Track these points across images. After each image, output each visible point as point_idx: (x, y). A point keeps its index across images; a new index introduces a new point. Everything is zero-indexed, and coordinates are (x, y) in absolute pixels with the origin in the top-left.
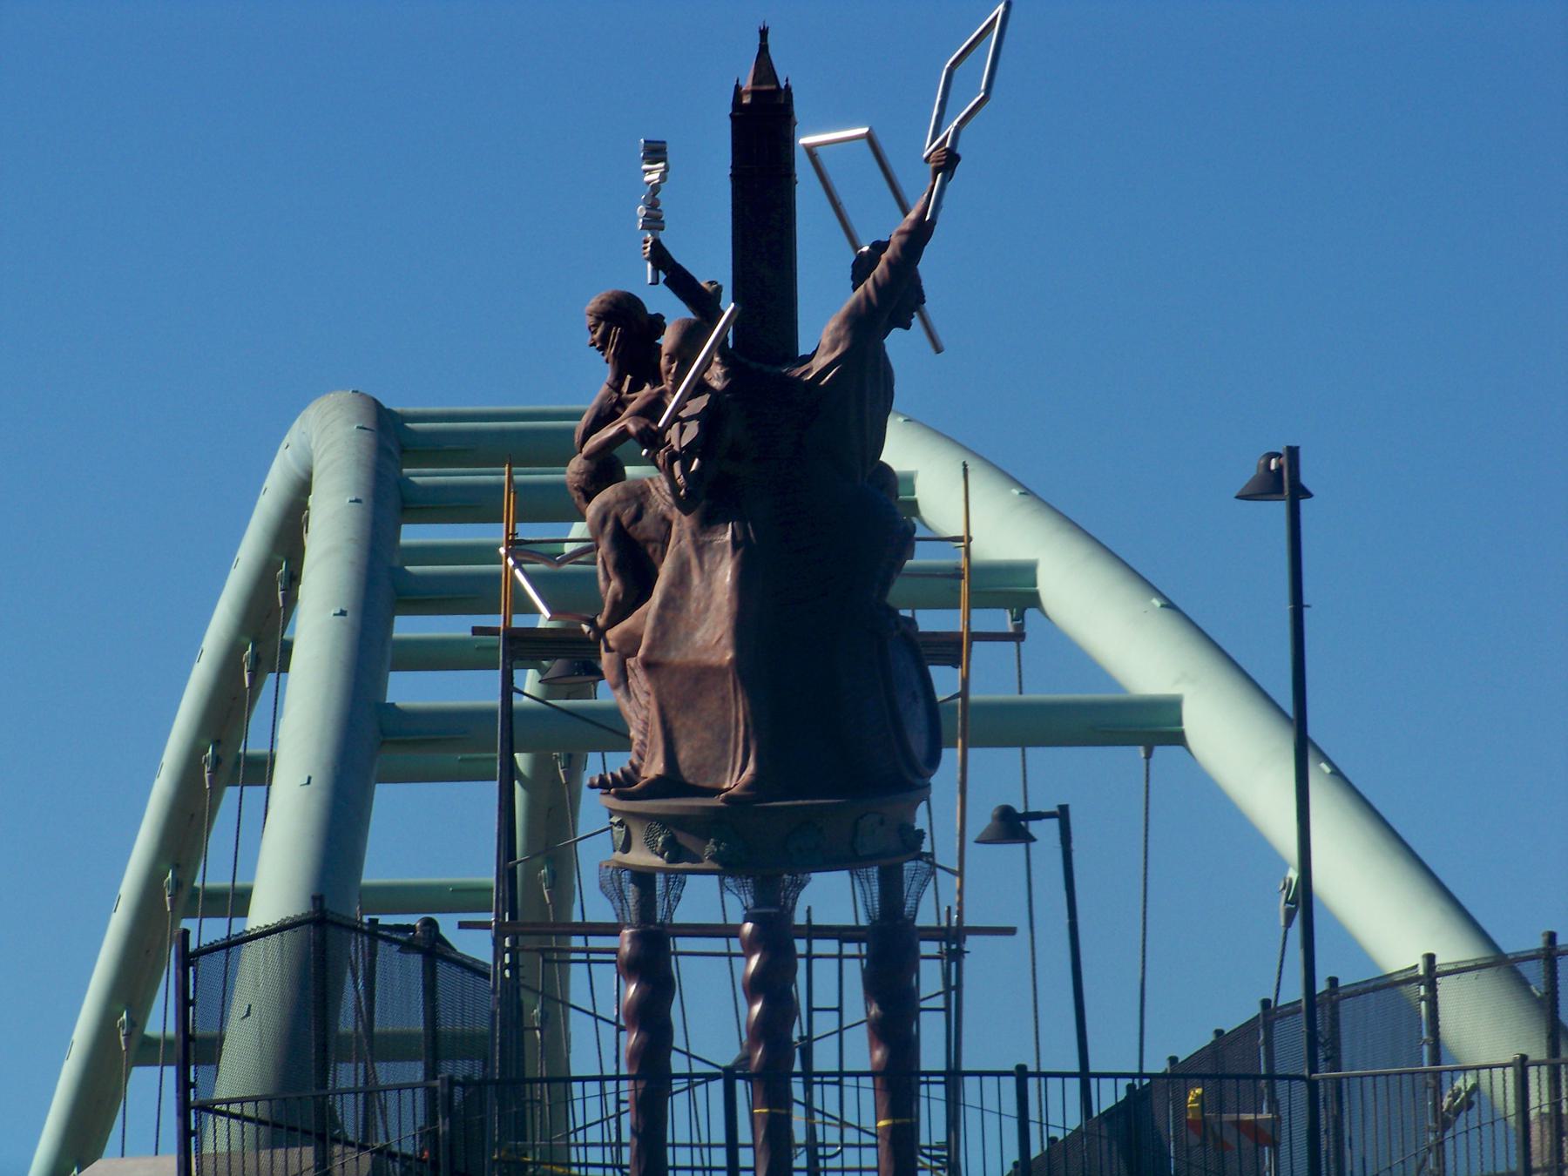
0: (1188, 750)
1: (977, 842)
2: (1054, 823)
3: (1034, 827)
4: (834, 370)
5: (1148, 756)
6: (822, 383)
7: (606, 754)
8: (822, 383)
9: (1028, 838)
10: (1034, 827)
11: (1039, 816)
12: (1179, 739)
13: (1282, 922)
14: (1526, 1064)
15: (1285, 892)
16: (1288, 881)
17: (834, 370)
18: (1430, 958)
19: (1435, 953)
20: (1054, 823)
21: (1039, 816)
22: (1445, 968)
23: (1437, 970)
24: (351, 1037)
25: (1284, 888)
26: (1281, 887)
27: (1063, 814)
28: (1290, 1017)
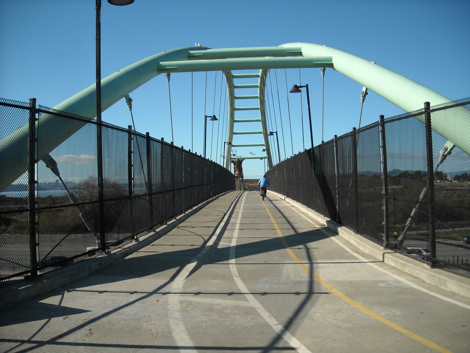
0: (334, 69)
1: (290, 92)
2: (305, 88)
3: (274, 134)
4: (21, 288)
5: (324, 71)
6: (20, 289)
7: (193, 72)
8: (20, 289)
9: (300, 91)
10: (274, 134)
11: (274, 132)
12: (331, 65)
13: (362, 102)
14: (429, 111)
15: (362, 94)
16: (363, 91)
17: (21, 288)
18: (382, 117)
19: (384, 115)
20: (305, 88)
21: (274, 132)
22: (387, 120)
23: (385, 121)
24: (66, 196)
25: (362, 93)
26: (361, 93)
27: (277, 132)
28: (373, 128)
